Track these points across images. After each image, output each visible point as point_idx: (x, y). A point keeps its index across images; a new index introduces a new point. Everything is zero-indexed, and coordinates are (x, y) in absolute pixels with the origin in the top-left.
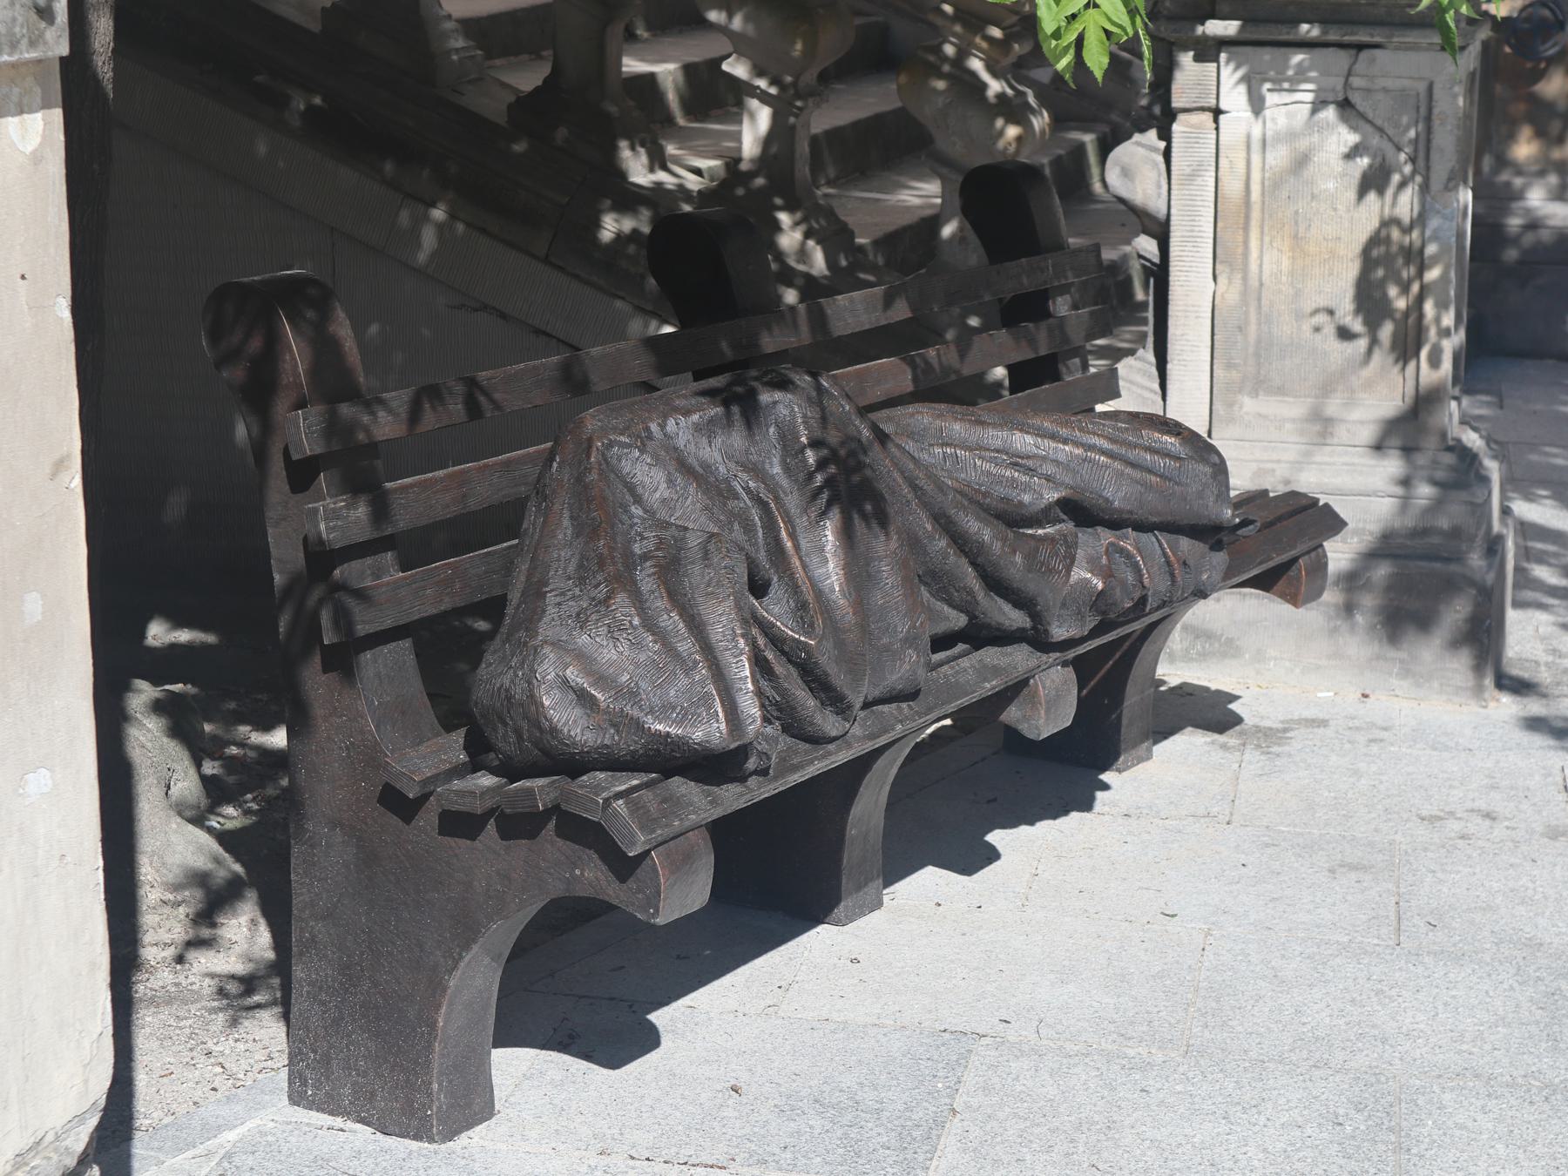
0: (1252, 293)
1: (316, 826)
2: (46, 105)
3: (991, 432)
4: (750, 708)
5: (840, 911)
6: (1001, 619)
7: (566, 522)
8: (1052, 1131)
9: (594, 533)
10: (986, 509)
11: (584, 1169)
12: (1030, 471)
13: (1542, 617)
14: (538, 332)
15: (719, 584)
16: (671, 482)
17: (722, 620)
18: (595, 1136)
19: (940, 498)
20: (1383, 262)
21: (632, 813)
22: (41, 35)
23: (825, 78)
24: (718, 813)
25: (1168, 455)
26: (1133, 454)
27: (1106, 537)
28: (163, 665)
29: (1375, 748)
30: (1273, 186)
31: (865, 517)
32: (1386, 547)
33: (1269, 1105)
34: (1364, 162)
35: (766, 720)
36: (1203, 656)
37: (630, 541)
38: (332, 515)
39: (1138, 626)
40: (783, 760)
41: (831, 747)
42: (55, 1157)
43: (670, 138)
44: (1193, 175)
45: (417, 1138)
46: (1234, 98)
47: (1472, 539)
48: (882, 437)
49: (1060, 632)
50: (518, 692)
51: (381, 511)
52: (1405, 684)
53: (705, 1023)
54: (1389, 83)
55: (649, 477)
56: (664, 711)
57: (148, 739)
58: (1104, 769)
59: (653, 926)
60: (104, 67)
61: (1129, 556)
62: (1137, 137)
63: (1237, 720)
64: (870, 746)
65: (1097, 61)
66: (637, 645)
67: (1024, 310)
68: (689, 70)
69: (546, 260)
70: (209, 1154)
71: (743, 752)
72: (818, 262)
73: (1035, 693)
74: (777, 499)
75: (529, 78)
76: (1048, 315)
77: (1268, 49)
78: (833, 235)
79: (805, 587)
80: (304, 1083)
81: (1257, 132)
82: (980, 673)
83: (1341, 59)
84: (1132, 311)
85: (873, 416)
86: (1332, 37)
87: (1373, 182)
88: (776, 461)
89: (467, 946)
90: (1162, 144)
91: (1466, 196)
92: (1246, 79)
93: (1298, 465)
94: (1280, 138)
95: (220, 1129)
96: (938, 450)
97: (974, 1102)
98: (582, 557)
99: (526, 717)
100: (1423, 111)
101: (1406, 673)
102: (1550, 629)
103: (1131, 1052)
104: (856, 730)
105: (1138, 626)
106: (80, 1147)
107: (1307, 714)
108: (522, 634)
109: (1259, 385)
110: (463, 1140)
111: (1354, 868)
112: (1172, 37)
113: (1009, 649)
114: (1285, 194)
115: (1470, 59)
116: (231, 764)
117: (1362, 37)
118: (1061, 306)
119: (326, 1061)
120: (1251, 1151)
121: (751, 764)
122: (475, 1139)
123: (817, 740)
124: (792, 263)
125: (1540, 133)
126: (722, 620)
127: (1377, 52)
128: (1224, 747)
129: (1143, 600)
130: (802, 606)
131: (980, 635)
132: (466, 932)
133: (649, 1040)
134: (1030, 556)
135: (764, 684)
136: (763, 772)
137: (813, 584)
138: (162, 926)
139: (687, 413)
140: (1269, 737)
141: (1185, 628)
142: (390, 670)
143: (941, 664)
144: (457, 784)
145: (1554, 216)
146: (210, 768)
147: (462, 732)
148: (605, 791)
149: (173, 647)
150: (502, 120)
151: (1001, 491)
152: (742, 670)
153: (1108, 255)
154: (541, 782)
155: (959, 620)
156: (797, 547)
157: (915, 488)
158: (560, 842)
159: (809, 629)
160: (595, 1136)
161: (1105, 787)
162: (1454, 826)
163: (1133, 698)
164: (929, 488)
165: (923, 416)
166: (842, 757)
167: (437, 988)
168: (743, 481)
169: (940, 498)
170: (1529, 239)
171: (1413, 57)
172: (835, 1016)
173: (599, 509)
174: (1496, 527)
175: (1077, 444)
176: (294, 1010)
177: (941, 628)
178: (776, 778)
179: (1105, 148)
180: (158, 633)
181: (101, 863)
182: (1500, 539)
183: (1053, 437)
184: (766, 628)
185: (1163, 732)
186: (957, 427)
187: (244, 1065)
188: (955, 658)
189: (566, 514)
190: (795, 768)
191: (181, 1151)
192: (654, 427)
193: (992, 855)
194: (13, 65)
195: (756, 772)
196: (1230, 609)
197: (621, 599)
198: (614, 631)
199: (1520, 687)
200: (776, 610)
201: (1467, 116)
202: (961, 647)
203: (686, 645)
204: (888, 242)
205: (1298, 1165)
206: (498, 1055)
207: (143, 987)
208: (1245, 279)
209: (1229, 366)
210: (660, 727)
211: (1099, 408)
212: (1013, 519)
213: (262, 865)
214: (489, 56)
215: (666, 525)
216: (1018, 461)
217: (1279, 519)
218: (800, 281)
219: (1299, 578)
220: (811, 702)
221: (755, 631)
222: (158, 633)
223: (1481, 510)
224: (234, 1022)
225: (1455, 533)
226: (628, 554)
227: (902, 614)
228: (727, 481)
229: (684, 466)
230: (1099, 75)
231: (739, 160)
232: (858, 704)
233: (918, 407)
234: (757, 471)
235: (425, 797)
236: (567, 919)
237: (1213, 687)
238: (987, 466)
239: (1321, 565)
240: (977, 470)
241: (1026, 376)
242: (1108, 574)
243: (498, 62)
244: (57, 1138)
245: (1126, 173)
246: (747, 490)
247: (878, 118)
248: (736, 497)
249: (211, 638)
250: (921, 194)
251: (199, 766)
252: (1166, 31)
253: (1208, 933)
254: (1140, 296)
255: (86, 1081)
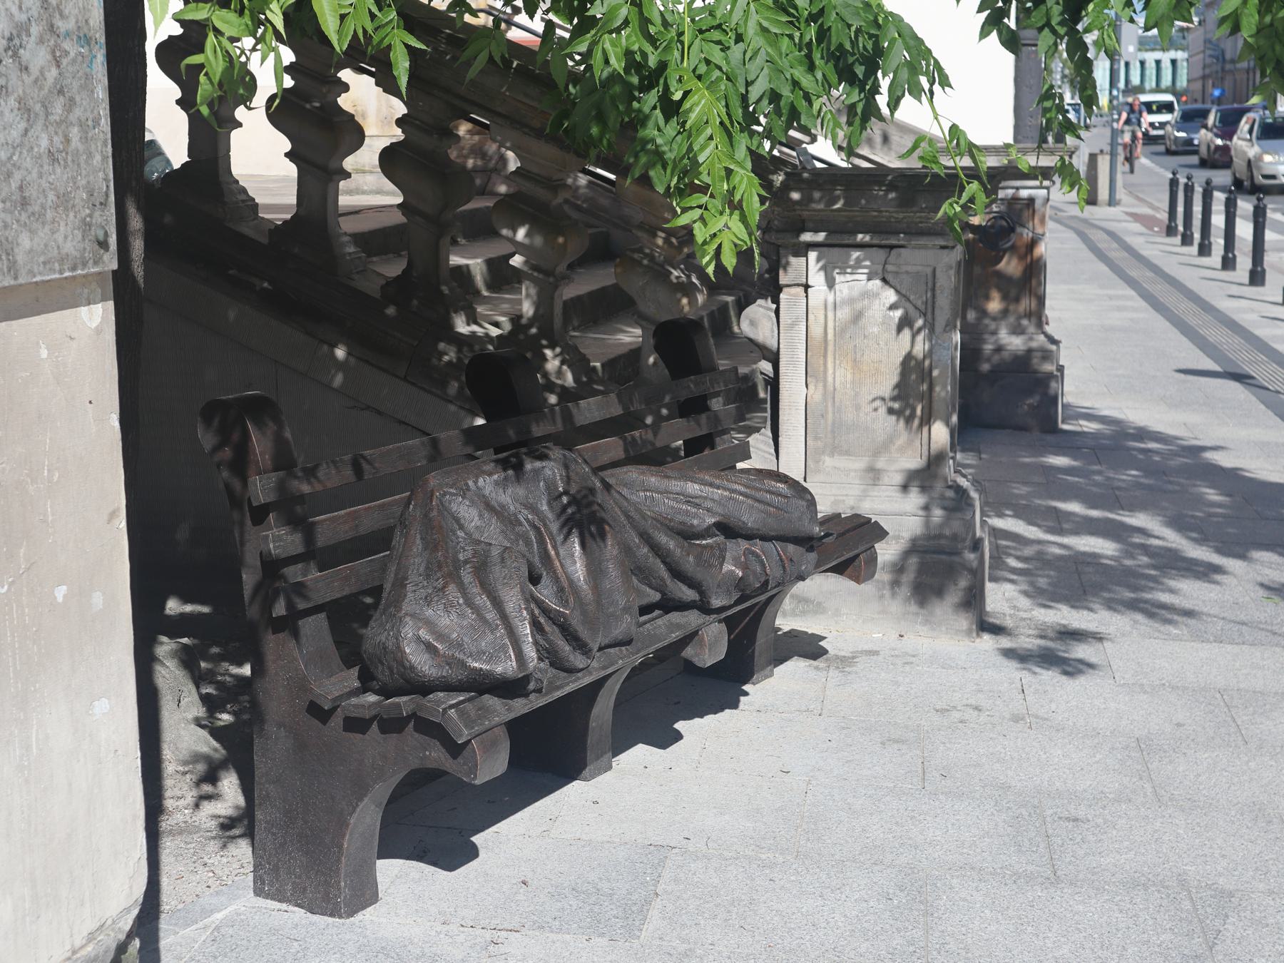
0: (830, 395)
1: (271, 728)
2: (104, 299)
3: (674, 482)
4: (530, 652)
5: (586, 773)
6: (680, 595)
7: (418, 541)
8: (717, 906)
9: (435, 548)
10: (671, 529)
11: (433, 933)
12: (697, 506)
13: (1008, 587)
14: (401, 422)
15: (511, 578)
16: (481, 516)
17: (513, 600)
18: (440, 913)
19: (643, 523)
20: (913, 375)
21: (460, 717)
22: (101, 258)
23: (571, 267)
24: (512, 716)
25: (780, 495)
26: (759, 495)
27: (744, 545)
28: (176, 627)
29: (907, 668)
30: (841, 332)
31: (592, 535)
32: (914, 548)
33: (848, 888)
34: (898, 313)
35: (540, 659)
36: (803, 613)
37: (457, 553)
38: (277, 539)
39: (763, 598)
40: (550, 683)
41: (580, 675)
42: (112, 934)
43: (481, 304)
44: (792, 325)
45: (332, 915)
46: (817, 280)
47: (964, 540)
48: (607, 487)
49: (716, 602)
50: (390, 645)
51: (309, 537)
52: (925, 628)
53: (507, 842)
54: (909, 268)
55: (468, 513)
56: (478, 655)
57: (169, 674)
58: (745, 683)
59: (474, 786)
60: (138, 270)
61: (758, 556)
62: (760, 302)
63: (825, 652)
64: (603, 673)
65: (729, 261)
66: (462, 616)
67: (693, 407)
68: (490, 263)
69: (405, 379)
70: (205, 928)
71: (527, 679)
72: (569, 379)
73: (702, 640)
74: (545, 525)
75: (393, 269)
76: (707, 409)
77: (836, 250)
78: (575, 360)
79: (563, 578)
80: (263, 883)
81: (831, 298)
82: (666, 627)
83: (880, 254)
84: (757, 404)
85: (606, 474)
86: (876, 242)
87: (904, 323)
88: (544, 502)
89: (361, 799)
90: (774, 306)
91: (957, 337)
92: (824, 268)
93: (864, 496)
94: (844, 302)
95: (212, 912)
96: (642, 494)
97: (669, 889)
98: (428, 562)
99: (395, 659)
100: (930, 285)
101: (927, 622)
102: (1016, 594)
103: (763, 857)
104: (595, 664)
105: (763, 598)
106: (128, 928)
107: (866, 647)
108: (392, 609)
109: (835, 450)
110: (359, 916)
111: (896, 741)
112: (779, 242)
113: (686, 613)
114: (848, 336)
115: (958, 253)
116: (220, 686)
117: (894, 242)
118: (716, 404)
119: (276, 869)
120: (837, 916)
121: (532, 686)
122: (367, 915)
123: (571, 671)
124: (553, 379)
125: (1005, 297)
126: (513, 600)
127: (902, 250)
128: (817, 668)
129: (766, 582)
130: (561, 590)
131: (668, 605)
132: (360, 789)
133: (471, 853)
134: (698, 557)
135: (538, 637)
136: (539, 691)
137: (568, 577)
138: (178, 791)
139: (490, 474)
140: (845, 662)
141: (792, 596)
142: (315, 628)
143: (645, 623)
144: (354, 700)
145: (1011, 344)
146: (208, 690)
147: (357, 668)
148: (445, 705)
149: (182, 615)
150: (377, 295)
151: (680, 518)
152: (526, 630)
153: (743, 370)
154: (405, 699)
155: (656, 597)
156: (557, 554)
157: (628, 517)
158: (416, 735)
159: (565, 603)
160: (440, 913)
161: (746, 694)
162: (956, 715)
163: (762, 639)
164: (637, 517)
165: (633, 473)
166: (587, 680)
167: (342, 825)
168: (524, 515)
169: (643, 523)
170: (996, 358)
171: (923, 252)
172: (584, 837)
173: (438, 533)
174: (978, 533)
175: (725, 489)
176: (257, 838)
177: (645, 601)
178: (547, 694)
179: (741, 306)
180: (173, 606)
181: (139, 754)
182: (981, 540)
183: (711, 485)
184: (539, 604)
185: (780, 660)
186: (653, 479)
187: (226, 871)
188: (653, 619)
189: (418, 536)
190: (558, 688)
191: (189, 925)
192: (470, 483)
193: (678, 736)
194: (84, 276)
195: (534, 691)
196: (820, 585)
197: (452, 588)
198: (448, 607)
199: (997, 630)
200: (545, 592)
201: (956, 289)
202: (657, 612)
203: (491, 615)
204: (609, 365)
205: (865, 925)
206: (381, 864)
207: (166, 824)
208: (825, 386)
209: (816, 438)
210: (476, 665)
211: (740, 465)
212: (687, 535)
213: (237, 750)
214: (369, 256)
215: (478, 542)
216: (690, 500)
217: (848, 531)
218: (558, 390)
219: (860, 566)
220: (567, 648)
221: (533, 606)
222: (173, 606)
223: (970, 525)
224: (224, 846)
225: (955, 537)
226: (456, 560)
227: (623, 594)
228: (515, 515)
229: (489, 506)
230: (730, 270)
231: (520, 317)
232: (596, 648)
233: (630, 468)
234: (533, 509)
235: (334, 709)
236: (420, 781)
237: (810, 632)
238: (671, 503)
239: (873, 559)
240: (666, 505)
241: (694, 446)
242: (745, 567)
243: (375, 259)
244: (114, 922)
245: (753, 323)
246: (527, 520)
247: (603, 289)
248: (521, 524)
249: (205, 609)
250: (631, 336)
251: (198, 688)
252: (773, 237)
253: (809, 783)
254: (762, 395)
255: (131, 887)
